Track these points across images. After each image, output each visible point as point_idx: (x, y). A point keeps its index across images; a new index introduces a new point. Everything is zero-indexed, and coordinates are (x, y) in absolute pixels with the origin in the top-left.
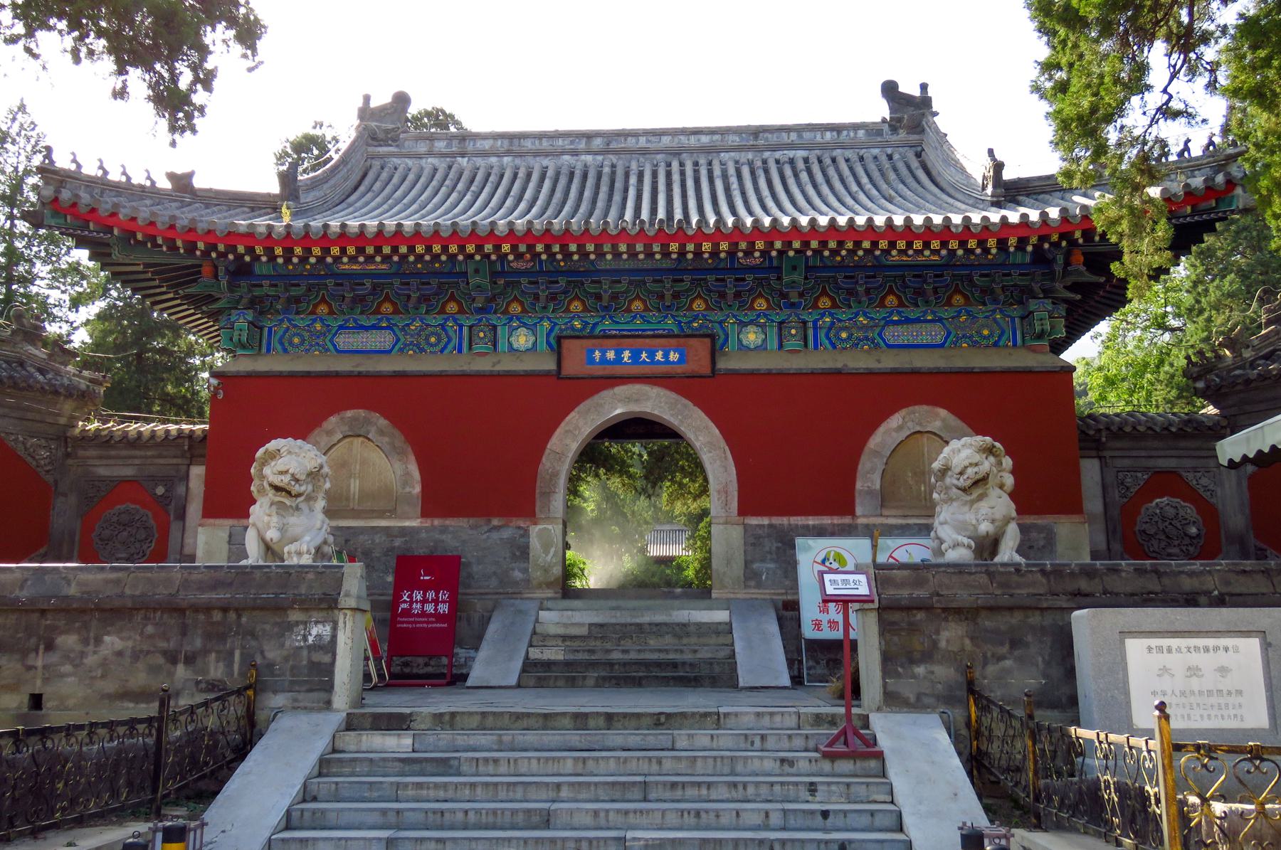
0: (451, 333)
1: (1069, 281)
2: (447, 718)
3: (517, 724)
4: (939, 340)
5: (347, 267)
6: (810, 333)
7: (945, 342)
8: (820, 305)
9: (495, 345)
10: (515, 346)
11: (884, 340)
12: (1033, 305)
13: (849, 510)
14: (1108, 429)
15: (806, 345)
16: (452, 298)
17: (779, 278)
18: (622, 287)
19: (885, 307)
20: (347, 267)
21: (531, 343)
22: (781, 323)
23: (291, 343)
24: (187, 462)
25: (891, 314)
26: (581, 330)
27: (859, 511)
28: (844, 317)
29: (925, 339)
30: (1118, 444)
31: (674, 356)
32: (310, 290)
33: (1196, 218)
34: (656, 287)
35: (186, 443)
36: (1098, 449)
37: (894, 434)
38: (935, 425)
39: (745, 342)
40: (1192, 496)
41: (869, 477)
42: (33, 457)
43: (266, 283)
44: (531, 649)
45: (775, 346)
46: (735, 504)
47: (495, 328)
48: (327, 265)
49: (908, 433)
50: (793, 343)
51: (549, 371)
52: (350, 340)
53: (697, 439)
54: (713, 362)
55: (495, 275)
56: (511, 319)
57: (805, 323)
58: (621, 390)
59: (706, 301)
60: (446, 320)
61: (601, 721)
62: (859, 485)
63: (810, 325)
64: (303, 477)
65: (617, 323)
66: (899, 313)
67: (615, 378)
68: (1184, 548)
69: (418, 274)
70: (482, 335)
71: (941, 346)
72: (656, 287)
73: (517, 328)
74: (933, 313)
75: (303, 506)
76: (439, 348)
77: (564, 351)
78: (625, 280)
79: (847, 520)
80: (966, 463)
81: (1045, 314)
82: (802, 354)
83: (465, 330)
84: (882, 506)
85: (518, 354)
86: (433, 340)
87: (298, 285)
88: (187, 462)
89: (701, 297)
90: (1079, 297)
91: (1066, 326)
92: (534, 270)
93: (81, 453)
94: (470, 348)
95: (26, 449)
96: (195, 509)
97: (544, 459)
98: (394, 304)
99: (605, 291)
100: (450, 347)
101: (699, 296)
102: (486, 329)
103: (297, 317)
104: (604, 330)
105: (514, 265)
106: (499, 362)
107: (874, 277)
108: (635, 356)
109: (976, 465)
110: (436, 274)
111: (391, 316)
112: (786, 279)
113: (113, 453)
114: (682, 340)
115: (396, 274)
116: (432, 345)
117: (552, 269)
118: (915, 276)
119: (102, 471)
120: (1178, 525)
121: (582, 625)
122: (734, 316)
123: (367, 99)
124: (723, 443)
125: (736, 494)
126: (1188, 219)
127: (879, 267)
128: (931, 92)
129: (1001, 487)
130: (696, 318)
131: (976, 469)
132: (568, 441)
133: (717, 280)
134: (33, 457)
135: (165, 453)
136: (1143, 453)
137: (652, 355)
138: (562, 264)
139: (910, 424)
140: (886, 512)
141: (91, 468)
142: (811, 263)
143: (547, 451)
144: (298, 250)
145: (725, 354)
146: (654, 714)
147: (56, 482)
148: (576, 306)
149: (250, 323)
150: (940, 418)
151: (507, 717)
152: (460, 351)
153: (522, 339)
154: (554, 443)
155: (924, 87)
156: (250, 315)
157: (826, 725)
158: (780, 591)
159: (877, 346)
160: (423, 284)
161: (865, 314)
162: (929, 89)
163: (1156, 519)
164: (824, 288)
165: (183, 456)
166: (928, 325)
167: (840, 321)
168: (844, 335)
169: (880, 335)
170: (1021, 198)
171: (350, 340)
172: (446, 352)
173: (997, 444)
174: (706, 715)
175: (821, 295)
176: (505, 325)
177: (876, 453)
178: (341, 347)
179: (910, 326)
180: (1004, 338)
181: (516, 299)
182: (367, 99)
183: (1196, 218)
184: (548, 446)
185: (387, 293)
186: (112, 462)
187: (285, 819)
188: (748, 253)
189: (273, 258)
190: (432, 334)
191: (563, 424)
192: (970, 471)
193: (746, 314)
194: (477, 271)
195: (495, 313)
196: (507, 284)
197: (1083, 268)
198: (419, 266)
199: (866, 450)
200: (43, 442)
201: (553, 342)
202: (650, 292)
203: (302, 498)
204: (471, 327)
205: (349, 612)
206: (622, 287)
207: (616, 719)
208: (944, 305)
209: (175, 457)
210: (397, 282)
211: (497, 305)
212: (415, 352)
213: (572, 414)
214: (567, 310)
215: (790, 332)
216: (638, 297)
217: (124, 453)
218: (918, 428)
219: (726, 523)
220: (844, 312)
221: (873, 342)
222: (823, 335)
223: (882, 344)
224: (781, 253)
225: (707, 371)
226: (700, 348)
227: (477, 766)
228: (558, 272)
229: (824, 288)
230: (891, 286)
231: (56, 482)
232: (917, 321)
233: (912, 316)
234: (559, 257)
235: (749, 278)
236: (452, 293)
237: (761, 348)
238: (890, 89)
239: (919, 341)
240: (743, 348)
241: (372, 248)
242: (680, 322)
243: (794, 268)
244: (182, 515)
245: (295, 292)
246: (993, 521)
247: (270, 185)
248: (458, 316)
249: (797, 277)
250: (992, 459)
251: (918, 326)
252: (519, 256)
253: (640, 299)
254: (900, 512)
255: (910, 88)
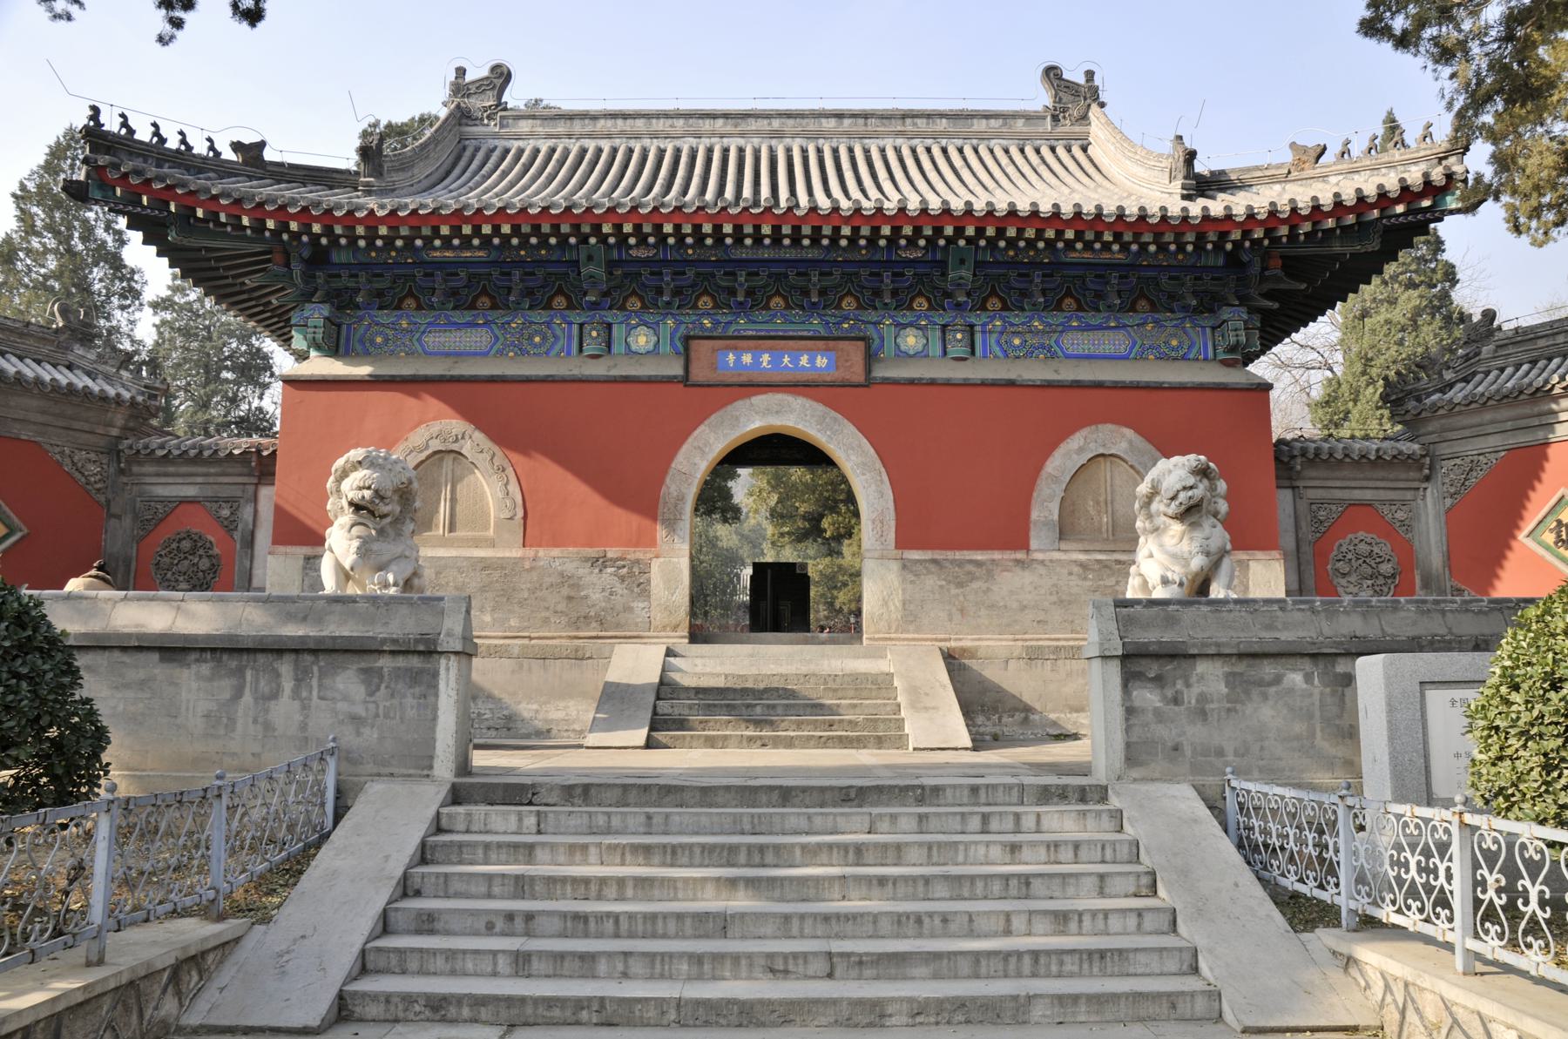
0: (558, 332)
1: (1266, 287)
2: (579, 791)
3: (667, 799)
4: (1122, 350)
5: (438, 254)
6: (978, 338)
7: (1130, 352)
8: (989, 306)
9: (609, 345)
10: (634, 347)
11: (1062, 349)
12: (1226, 313)
13: (1024, 545)
14: (1303, 455)
15: (973, 353)
16: (560, 292)
17: (944, 274)
18: (759, 282)
19: (1062, 310)
20: (438, 254)
21: (652, 344)
22: (944, 327)
23: (372, 342)
24: (255, 480)
25: (1070, 319)
26: (710, 330)
27: (1034, 544)
28: (1016, 321)
29: (1108, 348)
30: (1314, 473)
31: (821, 362)
32: (395, 282)
33: (1410, 218)
34: (801, 282)
35: (254, 458)
36: (1290, 478)
37: (1075, 456)
38: (1120, 448)
39: (903, 348)
40: (1388, 531)
41: (1045, 508)
42: (83, 474)
43: (344, 273)
44: (660, 703)
45: (939, 351)
46: (891, 536)
47: (609, 326)
48: (417, 250)
49: (1091, 455)
50: (956, 350)
51: (675, 377)
52: (442, 339)
53: (848, 459)
54: (868, 370)
55: (611, 265)
56: (629, 317)
57: (972, 326)
58: (760, 400)
59: (857, 299)
60: (552, 317)
61: (775, 796)
62: (1034, 515)
63: (978, 328)
64: (389, 494)
65: (754, 322)
66: (1079, 319)
67: (753, 386)
68: (1378, 589)
69: (521, 263)
70: (594, 334)
71: (1125, 358)
72: (801, 282)
73: (635, 327)
74: (1116, 319)
75: (390, 530)
76: (543, 350)
77: (693, 355)
78: (764, 273)
79: (1020, 555)
80: (1179, 486)
81: (1236, 322)
82: (968, 362)
83: (575, 328)
84: (1060, 539)
85: (637, 357)
86: (537, 339)
87: (381, 275)
88: (255, 480)
89: (852, 294)
90: (1276, 306)
91: (1261, 338)
92: (657, 258)
93: (135, 469)
94: (581, 350)
95: (74, 464)
96: (264, 536)
97: (668, 480)
98: (492, 298)
99: (741, 285)
100: (557, 348)
101: (849, 293)
102: (599, 327)
103: (380, 312)
104: (739, 331)
105: (633, 253)
106: (616, 365)
107: (1051, 275)
108: (776, 361)
109: (1191, 488)
110: (541, 262)
111: (487, 313)
112: (951, 275)
113: (171, 469)
114: (831, 343)
115: (493, 263)
116: (535, 346)
117: (679, 258)
118: (1096, 276)
119: (161, 491)
120: (1373, 563)
121: (718, 675)
122: (891, 317)
123: (461, 72)
124: (879, 464)
125: (893, 523)
126: (1393, 220)
127: (1057, 265)
128: (1097, 81)
129: (1215, 515)
130: (846, 319)
131: (1190, 493)
132: (697, 460)
133: (872, 274)
134: (83, 474)
135: (230, 470)
136: (1338, 484)
137: (795, 360)
138: (690, 252)
139: (1092, 445)
140: (1063, 546)
141: (148, 487)
142: (980, 258)
143: (671, 472)
144: (383, 231)
145: (882, 360)
146: (841, 789)
147: (108, 502)
148: (705, 302)
149: (326, 318)
150: (1121, 440)
151: (655, 791)
152: (569, 354)
153: (642, 340)
154: (680, 461)
155: (1090, 75)
156: (326, 310)
157: (1055, 800)
158: (942, 636)
159: (1053, 356)
160: (527, 274)
161: (1040, 319)
162: (1096, 78)
163: (1349, 556)
164: (993, 286)
165: (249, 475)
166: (1111, 333)
167: (1012, 325)
168: (1017, 342)
169: (1057, 342)
170: (1211, 193)
171: (442, 339)
172: (553, 353)
173: (1211, 464)
174: (907, 788)
175: (990, 295)
176: (621, 323)
177: (1055, 479)
178: (431, 349)
179: (1090, 333)
180: (1194, 351)
181: (634, 293)
182: (461, 72)
183: (1410, 218)
184: (673, 465)
185: (484, 285)
186: (170, 480)
187: (360, 961)
188: (912, 241)
189: (353, 240)
190: (537, 333)
191: (690, 440)
192: (1183, 496)
193: (904, 315)
194: (590, 258)
195: (610, 308)
196: (626, 275)
197: (1279, 272)
198: (523, 253)
199: (1043, 474)
200: (92, 456)
201: (679, 345)
202: (792, 287)
203: (388, 520)
204: (581, 326)
205: (453, 657)
206: (759, 282)
207: (794, 793)
208: (1128, 311)
209: (240, 475)
210: (496, 273)
211: (612, 300)
212: (516, 354)
213: (702, 428)
214: (695, 307)
215: (954, 337)
216: (778, 293)
217: (184, 469)
218: (1101, 451)
219: (882, 558)
220: (1017, 316)
221: (1049, 351)
222: (993, 341)
223: (1060, 354)
224: (950, 241)
225: (860, 378)
226: (855, 351)
227: (623, 854)
228: (686, 261)
229: (993, 286)
230: (1068, 288)
231: (108, 502)
232: (1099, 328)
233: (1093, 322)
234: (689, 240)
235: (909, 273)
236: (560, 285)
237: (922, 355)
238: (1052, 74)
239: (1101, 351)
240: (903, 356)
241: (470, 227)
242: (828, 323)
243: (962, 262)
244: (250, 542)
245: (379, 285)
246: (1208, 554)
247: (344, 157)
248: (567, 312)
249: (966, 273)
250: (1205, 481)
251: (1100, 333)
252: (642, 240)
253: (780, 295)
254: (1080, 546)
255: (1075, 75)
